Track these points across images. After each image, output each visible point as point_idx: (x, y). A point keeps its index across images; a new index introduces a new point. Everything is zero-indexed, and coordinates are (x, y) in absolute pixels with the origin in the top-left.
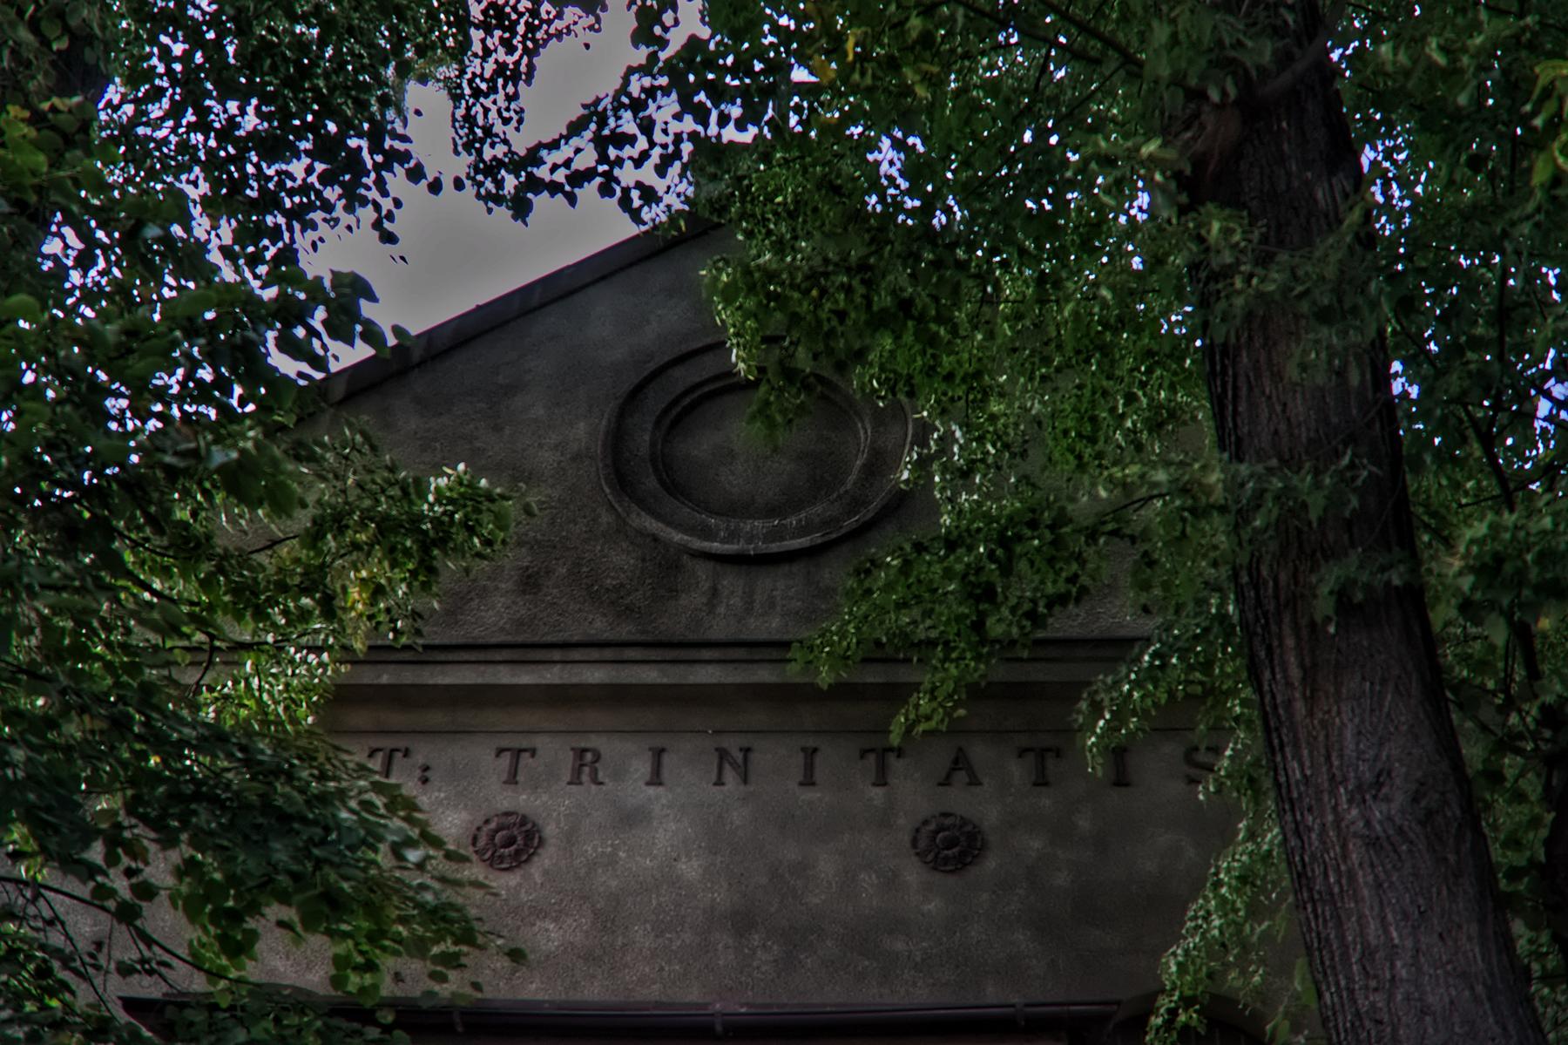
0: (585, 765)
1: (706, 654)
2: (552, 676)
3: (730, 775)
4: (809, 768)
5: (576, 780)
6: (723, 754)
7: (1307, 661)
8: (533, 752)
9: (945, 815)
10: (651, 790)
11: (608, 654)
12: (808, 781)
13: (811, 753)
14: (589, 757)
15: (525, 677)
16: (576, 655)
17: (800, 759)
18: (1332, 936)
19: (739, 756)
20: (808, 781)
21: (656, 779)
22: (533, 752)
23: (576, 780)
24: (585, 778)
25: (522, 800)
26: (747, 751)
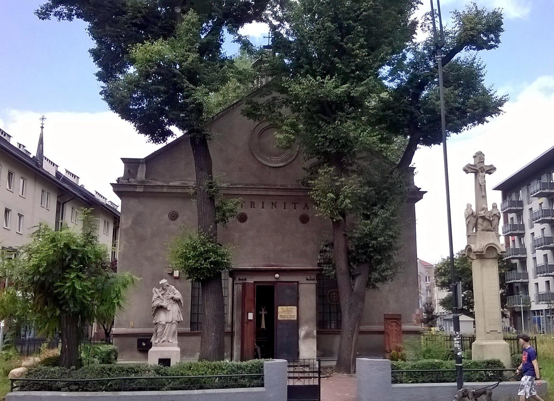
0: (252, 204)
3: (274, 207)
6: (273, 203)
21: (263, 208)
26: (276, 203)
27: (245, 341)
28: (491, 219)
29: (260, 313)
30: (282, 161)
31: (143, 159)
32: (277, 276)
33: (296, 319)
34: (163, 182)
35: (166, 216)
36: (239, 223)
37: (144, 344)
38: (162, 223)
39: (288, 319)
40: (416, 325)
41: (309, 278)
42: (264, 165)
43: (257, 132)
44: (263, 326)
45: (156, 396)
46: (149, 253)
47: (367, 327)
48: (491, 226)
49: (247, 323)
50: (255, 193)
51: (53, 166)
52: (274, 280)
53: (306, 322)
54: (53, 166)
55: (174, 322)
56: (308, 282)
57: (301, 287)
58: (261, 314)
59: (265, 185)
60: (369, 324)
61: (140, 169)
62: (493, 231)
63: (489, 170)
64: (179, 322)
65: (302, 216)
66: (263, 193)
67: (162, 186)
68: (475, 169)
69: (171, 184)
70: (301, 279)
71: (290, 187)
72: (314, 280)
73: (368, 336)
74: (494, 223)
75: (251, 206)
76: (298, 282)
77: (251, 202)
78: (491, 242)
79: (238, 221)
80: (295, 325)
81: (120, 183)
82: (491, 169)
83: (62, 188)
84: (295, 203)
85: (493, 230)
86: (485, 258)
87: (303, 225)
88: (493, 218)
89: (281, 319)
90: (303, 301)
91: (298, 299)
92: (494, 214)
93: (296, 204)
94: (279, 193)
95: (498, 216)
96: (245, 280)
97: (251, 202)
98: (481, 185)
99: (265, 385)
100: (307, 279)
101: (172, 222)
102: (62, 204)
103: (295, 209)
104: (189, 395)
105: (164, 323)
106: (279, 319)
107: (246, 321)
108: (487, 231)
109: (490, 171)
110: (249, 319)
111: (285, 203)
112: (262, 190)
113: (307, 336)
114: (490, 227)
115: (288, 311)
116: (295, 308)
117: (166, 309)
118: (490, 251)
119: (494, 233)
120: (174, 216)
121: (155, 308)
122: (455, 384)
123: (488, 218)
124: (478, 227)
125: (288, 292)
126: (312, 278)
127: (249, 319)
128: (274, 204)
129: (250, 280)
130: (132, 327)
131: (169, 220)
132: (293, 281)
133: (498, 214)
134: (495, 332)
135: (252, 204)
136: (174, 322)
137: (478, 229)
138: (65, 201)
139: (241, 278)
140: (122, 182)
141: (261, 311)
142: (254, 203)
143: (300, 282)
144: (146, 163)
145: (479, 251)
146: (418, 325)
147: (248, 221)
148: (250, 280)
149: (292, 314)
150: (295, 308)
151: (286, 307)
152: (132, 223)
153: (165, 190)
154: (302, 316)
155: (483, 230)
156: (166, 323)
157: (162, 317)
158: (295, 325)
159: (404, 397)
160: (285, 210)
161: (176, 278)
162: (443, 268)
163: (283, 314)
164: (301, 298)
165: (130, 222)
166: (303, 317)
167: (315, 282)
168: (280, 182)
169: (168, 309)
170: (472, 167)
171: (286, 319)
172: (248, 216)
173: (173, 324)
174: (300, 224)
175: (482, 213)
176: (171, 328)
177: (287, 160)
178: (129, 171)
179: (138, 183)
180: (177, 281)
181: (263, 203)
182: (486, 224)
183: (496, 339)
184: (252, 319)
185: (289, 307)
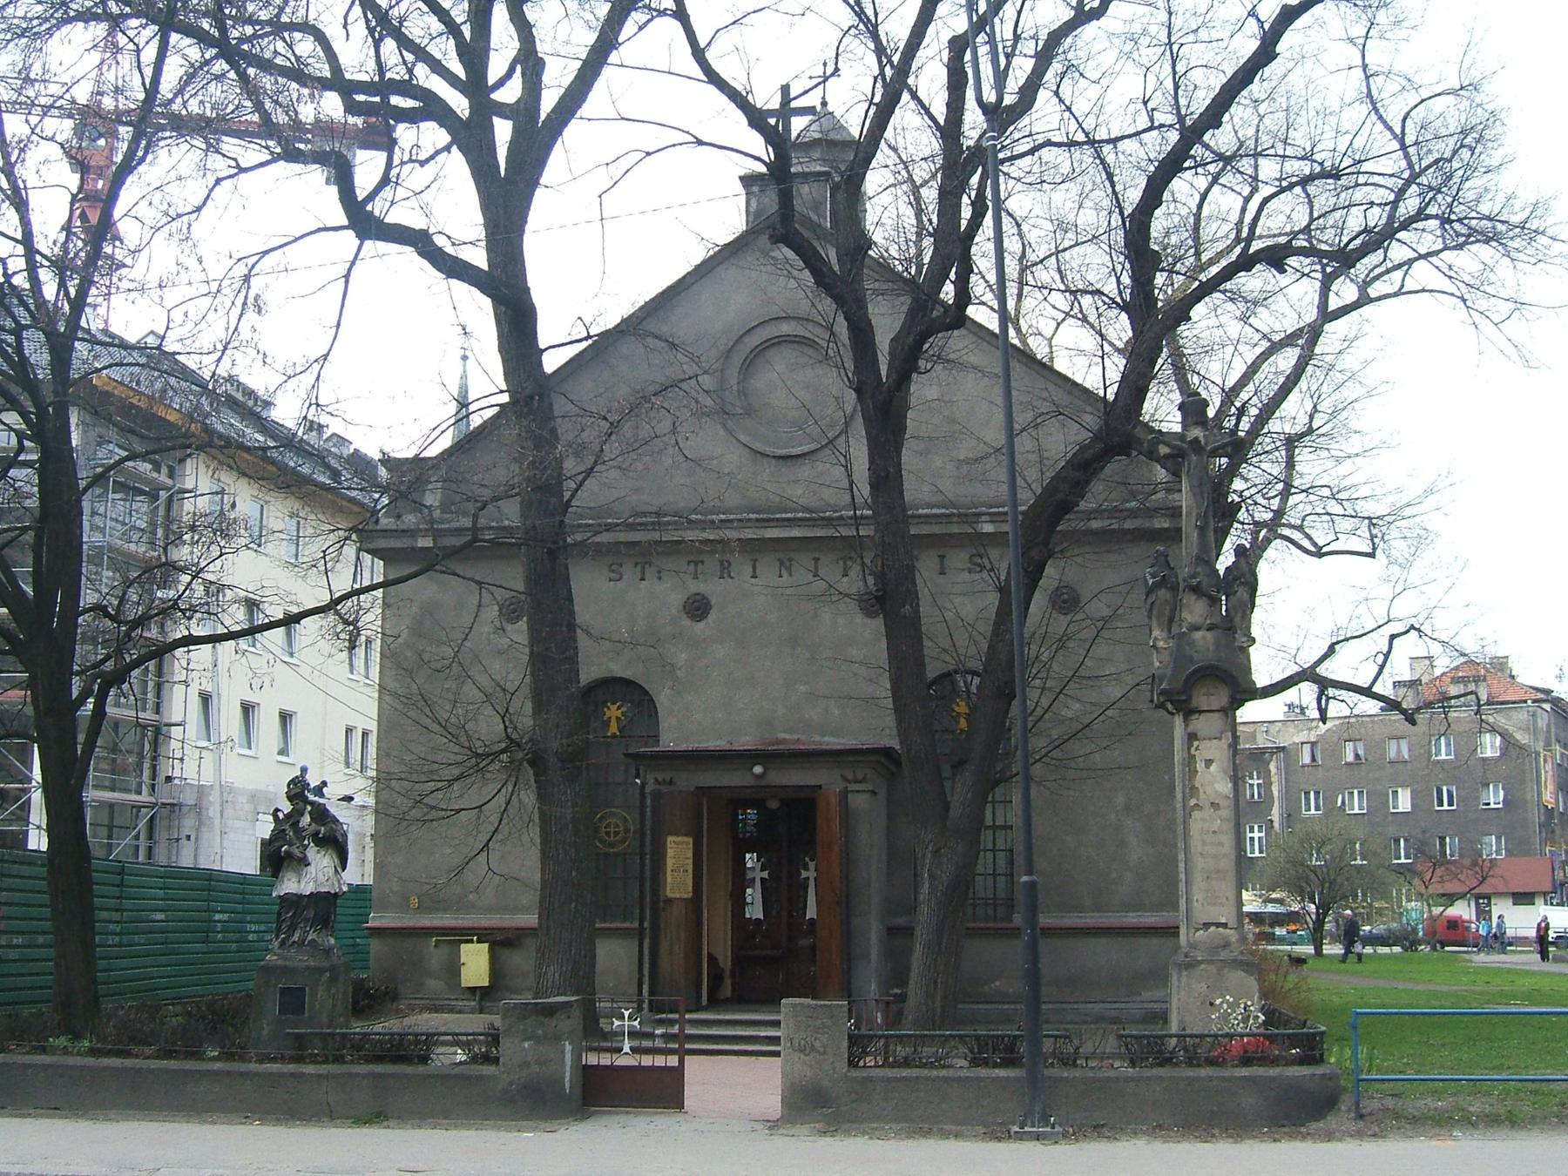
0: (725, 570)
1: (772, 524)
8: (702, 562)
21: (754, 576)
22: (702, 562)
25: (694, 587)
29: (804, 874)
32: (758, 769)
36: (686, 622)
75: (722, 572)
97: (721, 562)
139: (660, 779)
142: (730, 564)
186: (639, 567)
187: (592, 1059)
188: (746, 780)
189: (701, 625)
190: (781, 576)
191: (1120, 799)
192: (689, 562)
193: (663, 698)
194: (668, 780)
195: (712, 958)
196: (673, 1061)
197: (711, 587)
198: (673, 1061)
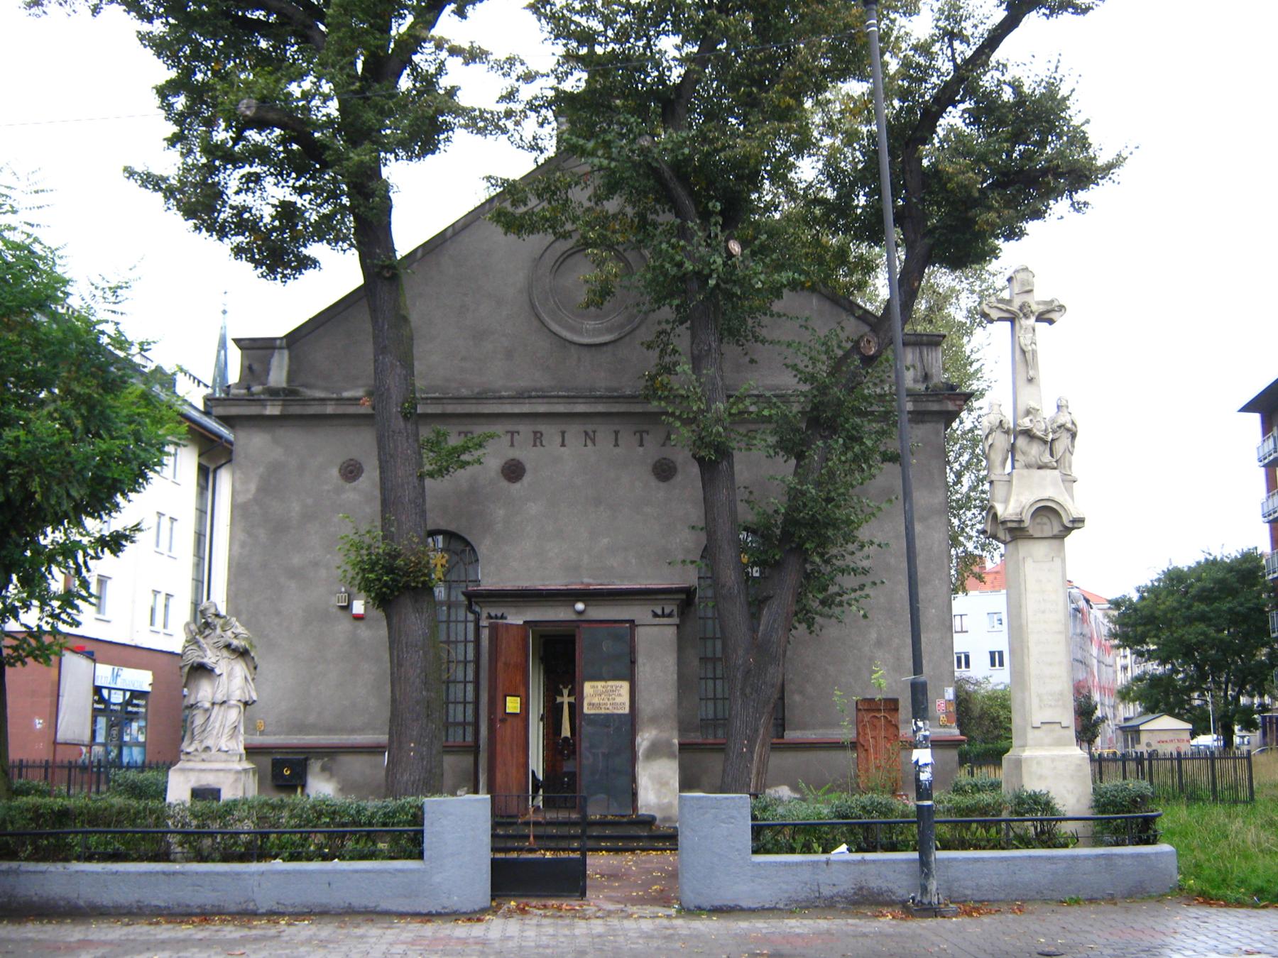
0: (538, 438)
1: (580, 400)
2: (526, 409)
3: (589, 442)
4: (616, 440)
5: (535, 445)
6: (586, 433)
7: (223, 352)
8: (518, 433)
9: (351, 460)
10: (563, 449)
11: (545, 400)
12: (616, 445)
13: (616, 433)
14: (539, 435)
15: (517, 409)
16: (552, 400)
17: (613, 436)
18: (741, 652)
19: (591, 434)
20: (616, 445)
21: (563, 445)
22: (518, 433)
23: (535, 445)
24: (538, 444)
25: (515, 454)
26: (594, 432)
27: (499, 760)
28: (1050, 437)
29: (559, 699)
30: (609, 330)
31: (281, 339)
32: (580, 606)
33: (627, 710)
34: (326, 389)
35: (335, 472)
36: (504, 484)
37: (287, 772)
38: (326, 487)
39: (608, 712)
40: (945, 726)
41: (659, 612)
42: (566, 340)
43: (549, 260)
44: (566, 731)
45: (157, 872)
46: (297, 560)
47: (821, 731)
48: (1052, 455)
49: (503, 721)
50: (542, 409)
51: (199, 385)
52: (574, 617)
53: (654, 720)
54: (199, 385)
55: (233, 702)
56: (657, 621)
57: (641, 633)
58: (562, 703)
59: (568, 390)
60: (804, 727)
61: (275, 362)
62: (1055, 468)
63: (1048, 312)
64: (246, 704)
65: (658, 461)
66: (561, 408)
67: (323, 400)
68: (1007, 311)
69: (346, 394)
70: (638, 612)
71: (628, 393)
72: (670, 615)
73: (822, 755)
74: (1060, 447)
75: (535, 441)
76: (633, 621)
77: (535, 433)
78: (1045, 496)
79: (502, 479)
80: (628, 724)
81: (230, 396)
82: (1052, 310)
83: (207, 434)
84: (641, 433)
85: (1055, 464)
86: (1031, 537)
87: (661, 484)
88: (1057, 435)
89: (592, 712)
90: (644, 669)
91: (633, 662)
92: (1058, 424)
93: (645, 435)
94: (600, 408)
95: (1068, 430)
96: (503, 617)
97: (535, 433)
98: (1024, 352)
99: (426, 854)
100: (655, 615)
101: (348, 486)
102: (211, 469)
103: (641, 445)
104: (238, 874)
105: (207, 705)
106: (586, 711)
107: (499, 715)
108: (1040, 468)
109: (1052, 316)
110: (508, 711)
111: (616, 433)
112: (560, 400)
113: (656, 751)
114: (1047, 458)
115: (609, 693)
116: (625, 686)
117: (212, 670)
118: (1045, 520)
119: (1056, 472)
120: (351, 472)
121: (186, 669)
122: (915, 855)
123: (1039, 434)
124: (1017, 458)
125: (607, 646)
126: (667, 611)
127: (508, 711)
128: (590, 437)
129: (516, 618)
130: (262, 733)
131: (341, 482)
132: (617, 618)
133: (1069, 425)
134: (1053, 726)
135: (538, 438)
136: (233, 702)
137: (1017, 465)
138: (219, 464)
139: (493, 614)
140: (236, 395)
141: (562, 695)
142: (542, 434)
143: (636, 623)
144: (289, 347)
145: (1013, 518)
146: (950, 727)
147: (527, 479)
148: (516, 618)
149: (618, 700)
150: (625, 686)
151: (603, 683)
152: (259, 490)
153: (330, 409)
154: (642, 705)
155: (1028, 466)
156: (213, 704)
157: (204, 692)
158: (628, 724)
159: (785, 887)
160: (617, 450)
161: (358, 618)
162: (1174, 628)
163: (596, 700)
164: (641, 660)
165: (253, 487)
166: (645, 708)
167: (675, 620)
168: (602, 380)
169: (218, 671)
170: (1000, 306)
171: (603, 711)
172: (528, 466)
173: (230, 707)
174: (654, 482)
175: (1026, 423)
176: (225, 717)
177: (622, 326)
178: (250, 368)
179: (271, 395)
180: (361, 624)
181: (563, 433)
182: (1035, 450)
183: (1059, 743)
184: (518, 711)
185: (610, 683)
186: (638, 434)
187: (920, 803)
188: (570, 615)
189: (518, 485)
190: (586, 445)
191: (874, 636)
192: (460, 433)
193: (483, 549)
194: (499, 615)
195: (533, 772)
196: (577, 855)
197: (525, 453)
198: (577, 855)
